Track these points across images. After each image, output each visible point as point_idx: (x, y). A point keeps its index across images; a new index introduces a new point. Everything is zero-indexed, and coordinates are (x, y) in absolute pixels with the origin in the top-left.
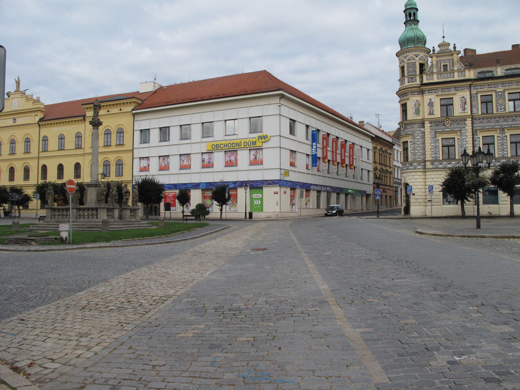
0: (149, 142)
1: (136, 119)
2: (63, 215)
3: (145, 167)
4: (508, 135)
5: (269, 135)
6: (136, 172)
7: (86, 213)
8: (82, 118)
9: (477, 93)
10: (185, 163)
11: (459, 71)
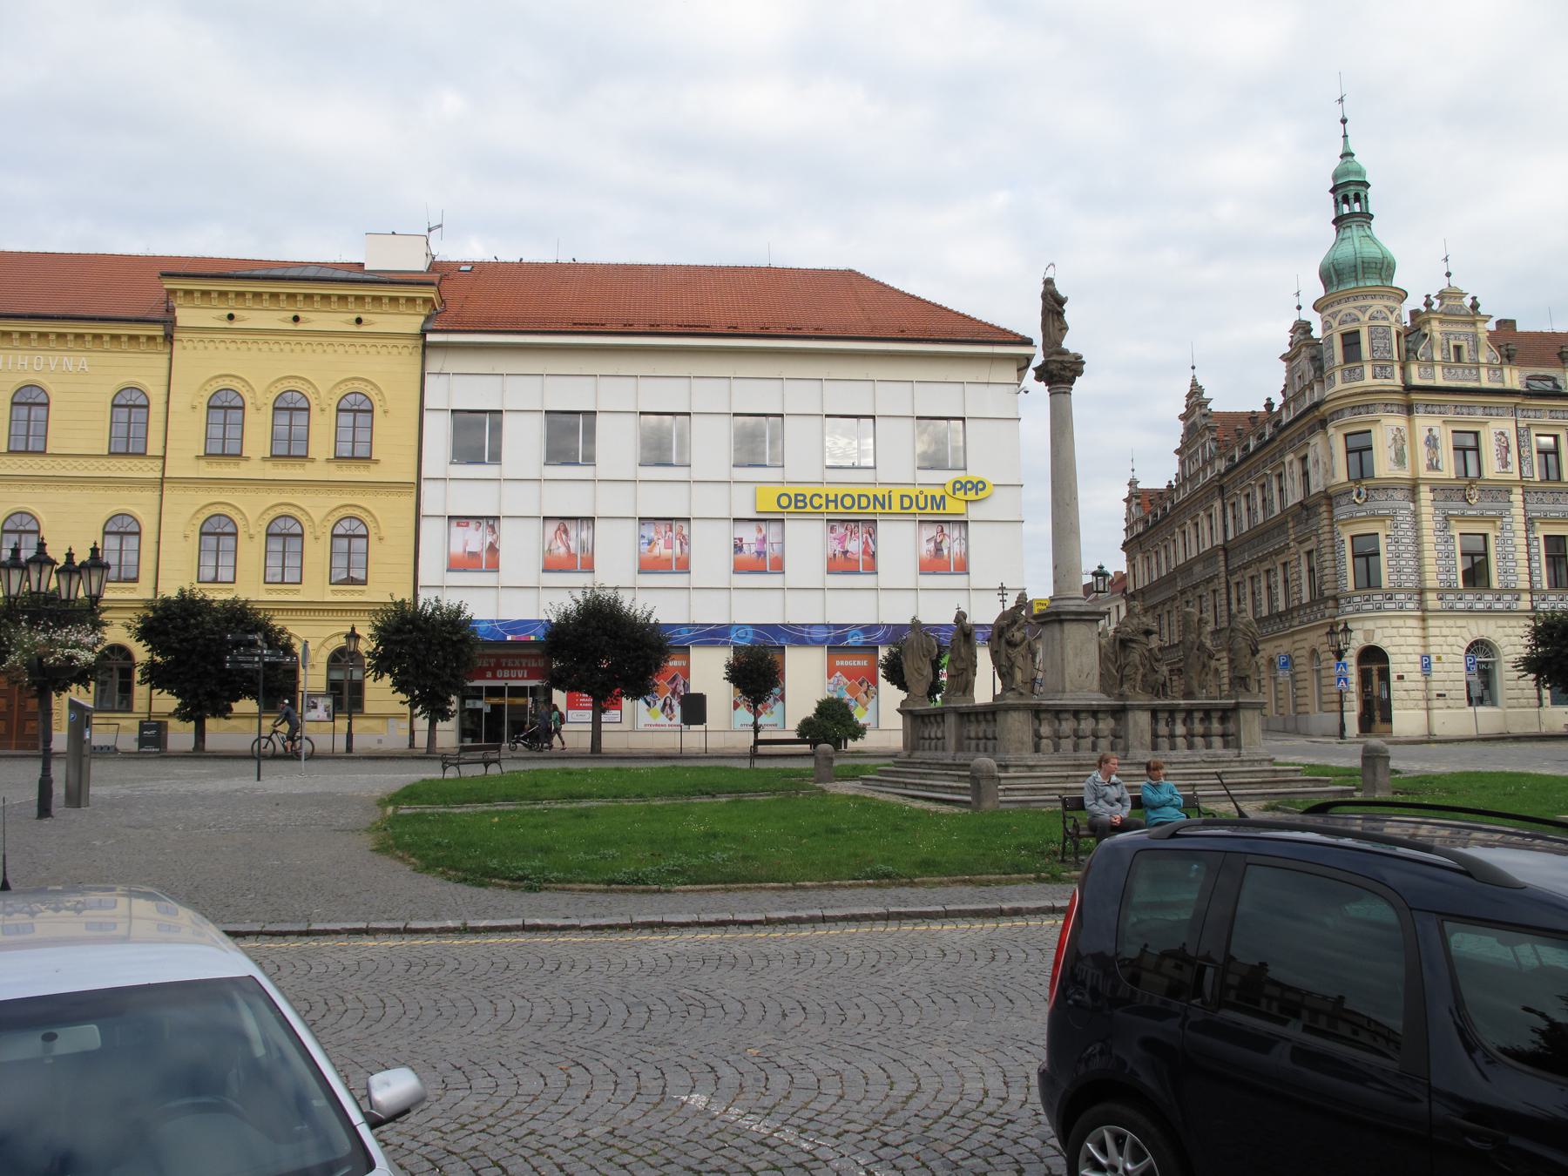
0: (496, 457)
1: (430, 367)
2: (1078, 735)
3: (473, 555)
4: (1456, 533)
5: (990, 480)
6: (432, 570)
7: (1067, 726)
8: (158, 331)
9: (1529, 427)
10: (660, 549)
11: (1489, 365)
